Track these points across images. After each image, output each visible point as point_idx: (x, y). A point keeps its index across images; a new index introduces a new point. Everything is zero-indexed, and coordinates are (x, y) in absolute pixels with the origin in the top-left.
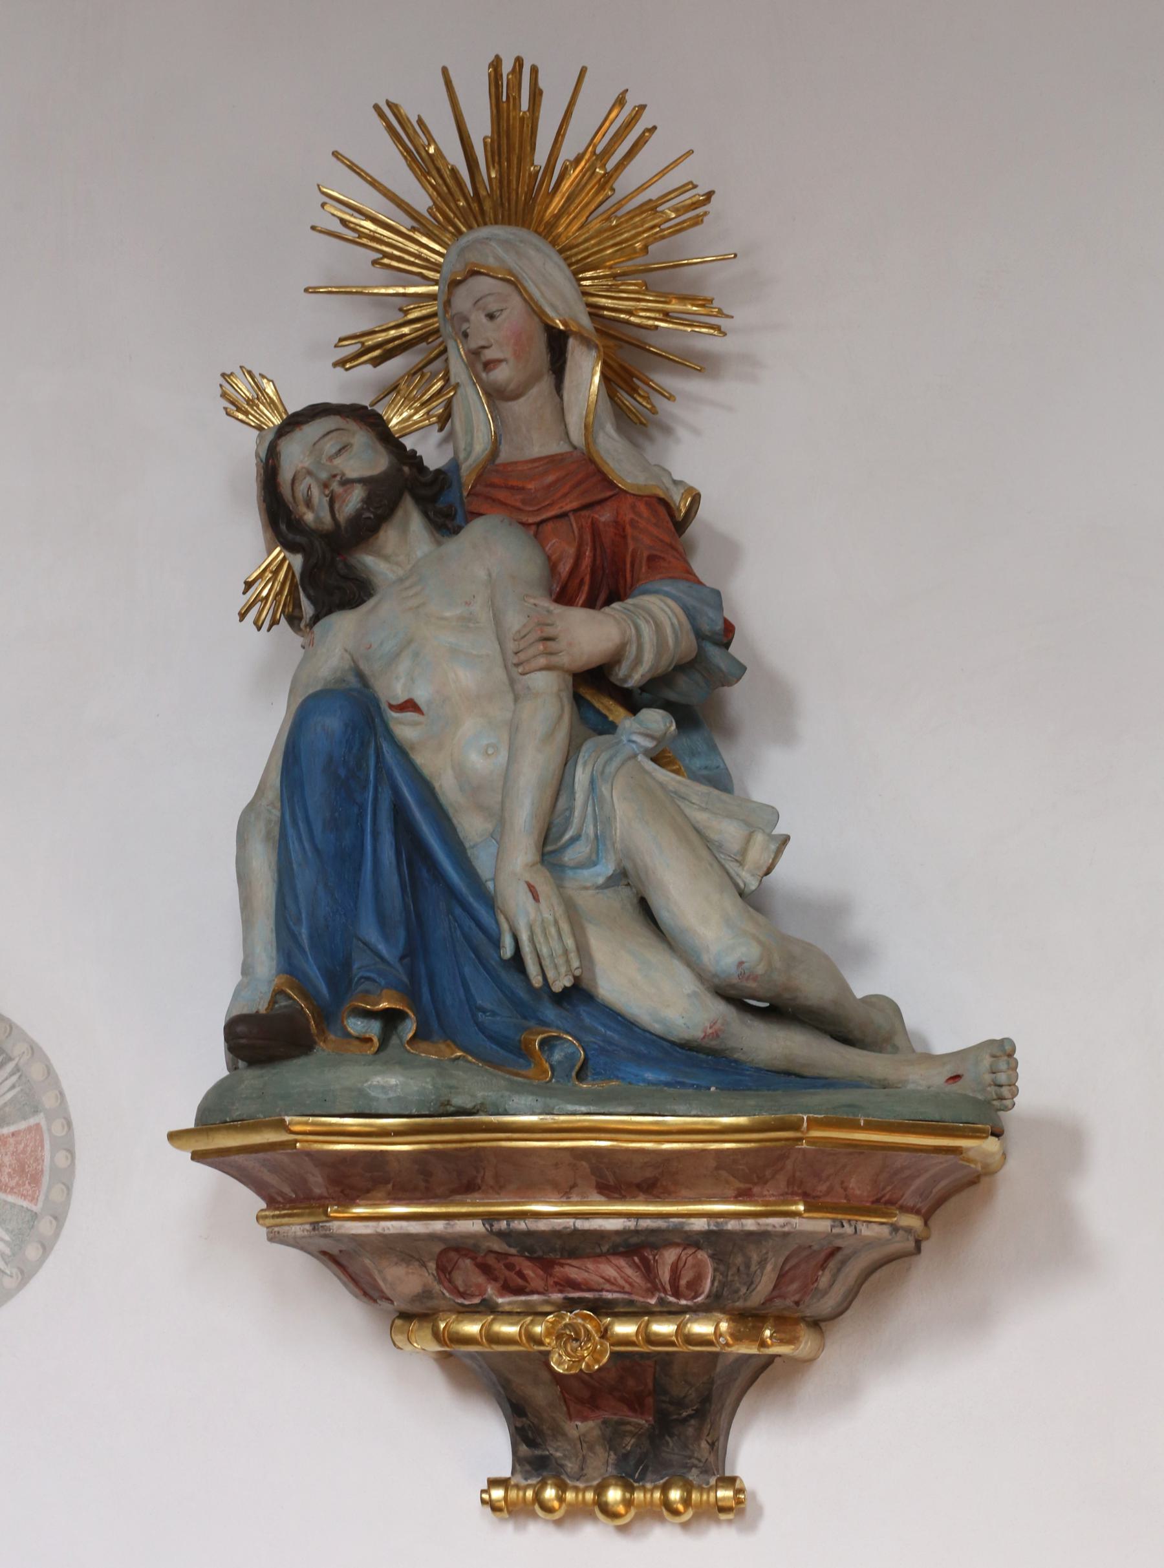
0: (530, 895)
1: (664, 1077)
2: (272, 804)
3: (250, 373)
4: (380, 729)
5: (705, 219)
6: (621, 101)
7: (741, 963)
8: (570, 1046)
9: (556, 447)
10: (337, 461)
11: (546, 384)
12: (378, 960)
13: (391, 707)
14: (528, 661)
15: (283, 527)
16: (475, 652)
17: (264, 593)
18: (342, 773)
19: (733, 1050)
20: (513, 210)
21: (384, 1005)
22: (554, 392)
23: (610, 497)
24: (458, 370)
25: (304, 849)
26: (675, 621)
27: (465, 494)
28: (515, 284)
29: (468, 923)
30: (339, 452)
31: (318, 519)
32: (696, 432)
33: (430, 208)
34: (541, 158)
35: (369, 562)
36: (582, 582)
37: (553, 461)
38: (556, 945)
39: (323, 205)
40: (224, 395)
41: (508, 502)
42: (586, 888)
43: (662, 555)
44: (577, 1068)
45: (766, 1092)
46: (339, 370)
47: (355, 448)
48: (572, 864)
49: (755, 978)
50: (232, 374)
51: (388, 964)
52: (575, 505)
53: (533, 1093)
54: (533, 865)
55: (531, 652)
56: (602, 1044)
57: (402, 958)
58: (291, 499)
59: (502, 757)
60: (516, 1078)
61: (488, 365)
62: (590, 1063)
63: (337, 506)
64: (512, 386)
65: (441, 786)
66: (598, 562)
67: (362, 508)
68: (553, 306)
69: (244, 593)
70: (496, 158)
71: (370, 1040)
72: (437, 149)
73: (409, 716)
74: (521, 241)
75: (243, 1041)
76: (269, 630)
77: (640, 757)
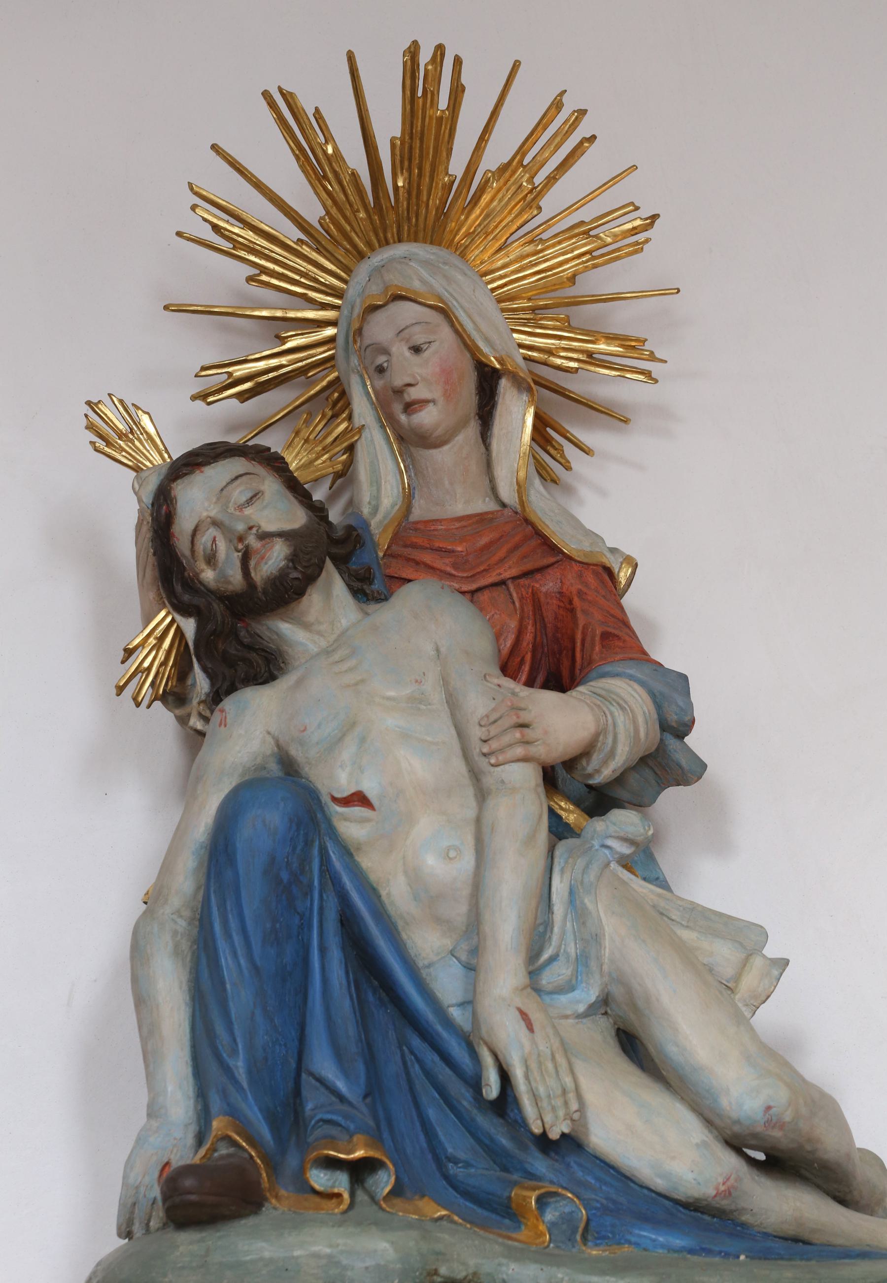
0: (523, 1024)
1: (678, 1242)
2: (178, 912)
3: (121, 402)
4: (323, 826)
5: (646, 247)
6: (557, 105)
7: (769, 1108)
8: (569, 1206)
9: (483, 505)
10: (248, 511)
11: (473, 429)
12: (334, 1099)
13: (334, 799)
14: (501, 750)
15: (178, 588)
16: (429, 739)
17: (146, 664)
18: (285, 876)
19: (743, 1210)
20: (421, 225)
21: (359, 1154)
22: (480, 440)
23: (553, 564)
24: (363, 409)
25: (239, 965)
26: (645, 709)
27: (381, 554)
28: (445, 312)
29: (431, 1058)
30: (250, 501)
31: (223, 578)
32: (602, 492)
33: (321, 218)
34: (457, 166)
35: (285, 630)
36: (522, 662)
37: (481, 519)
38: (552, 1082)
39: (194, 208)
40: (91, 427)
41: (435, 565)
42: (566, 1017)
43: (616, 632)
44: (580, 1230)
45: (799, 1262)
46: (199, 403)
47: (268, 496)
48: (549, 988)
49: (782, 1126)
50: (99, 402)
51: (350, 1104)
52: (514, 572)
53: (536, 1261)
54: (525, 988)
55: (506, 739)
56: (604, 1202)
57: (365, 1097)
58: (187, 553)
59: (467, 862)
60: (510, 1242)
61: (410, 407)
62: (593, 1224)
63: (252, 563)
64: (439, 432)
65: (389, 894)
66: (538, 639)
67: (288, 567)
68: (487, 340)
69: (123, 662)
70: (406, 163)
71: (339, 1195)
72: (336, 148)
73: (357, 811)
74: (445, 263)
75: (193, 1197)
76: (149, 707)
77: (613, 865)
